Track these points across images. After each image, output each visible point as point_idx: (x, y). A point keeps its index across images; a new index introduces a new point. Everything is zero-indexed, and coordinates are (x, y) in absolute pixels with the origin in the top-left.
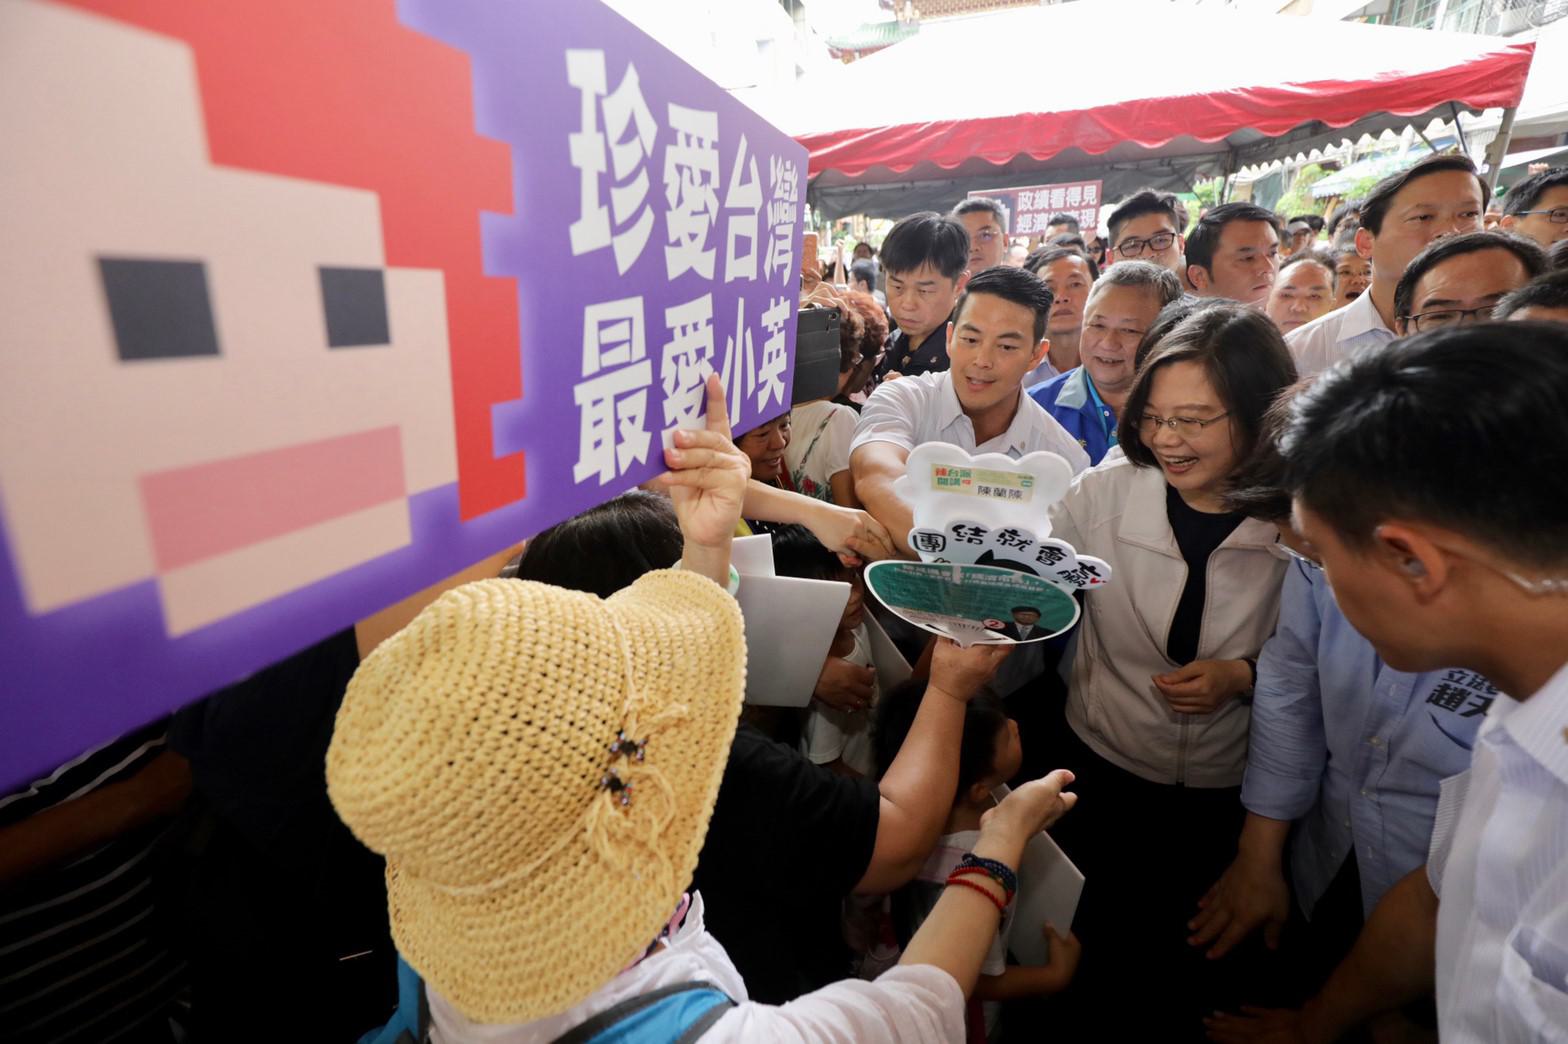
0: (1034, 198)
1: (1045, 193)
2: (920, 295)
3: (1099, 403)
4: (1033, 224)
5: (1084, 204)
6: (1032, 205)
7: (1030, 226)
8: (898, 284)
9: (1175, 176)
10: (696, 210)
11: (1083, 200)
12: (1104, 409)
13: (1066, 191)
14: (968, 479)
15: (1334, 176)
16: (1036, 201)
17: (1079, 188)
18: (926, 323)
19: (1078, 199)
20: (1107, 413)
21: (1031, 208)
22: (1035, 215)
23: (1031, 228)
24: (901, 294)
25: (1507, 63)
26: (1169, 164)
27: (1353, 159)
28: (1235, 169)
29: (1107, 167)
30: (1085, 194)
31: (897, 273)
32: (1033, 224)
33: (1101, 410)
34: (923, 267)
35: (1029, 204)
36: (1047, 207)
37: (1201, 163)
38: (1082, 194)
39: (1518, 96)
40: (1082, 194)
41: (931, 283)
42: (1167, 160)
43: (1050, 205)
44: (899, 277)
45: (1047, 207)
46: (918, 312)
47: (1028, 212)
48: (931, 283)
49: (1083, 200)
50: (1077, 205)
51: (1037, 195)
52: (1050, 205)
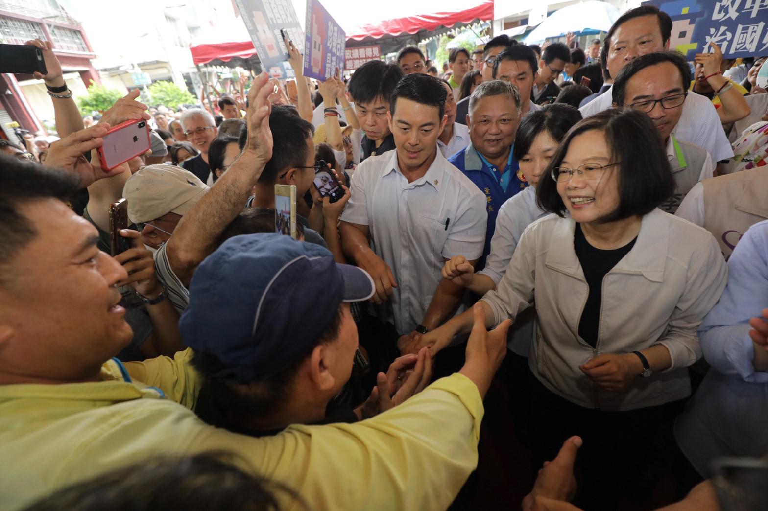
0: (352, 53)
1: (356, 51)
2: (377, 116)
3: (490, 165)
4: (353, 65)
5: (374, 56)
6: (352, 56)
7: (352, 65)
8: (362, 109)
9: (400, 45)
10: (445, 227)
11: (373, 54)
12: (492, 168)
13: (358, 51)
14: (207, 74)
15: (453, 41)
16: (353, 54)
17: (371, 49)
18: (383, 133)
19: (371, 54)
20: (495, 170)
21: (351, 58)
22: (354, 61)
23: (353, 67)
24: (365, 115)
25: (488, 6)
26: (396, 40)
27: (458, 33)
28: (420, 41)
29: (373, 43)
30: (374, 52)
31: (361, 102)
32: (353, 65)
33: (490, 169)
34: (376, 97)
35: (350, 55)
36: (358, 57)
37: (408, 39)
38: (372, 51)
39: (493, 16)
40: (372, 51)
41: (383, 107)
42: (395, 39)
43: (359, 56)
44: (362, 105)
45: (358, 57)
46: (376, 127)
47: (350, 59)
48: (383, 107)
49: (373, 54)
50: (371, 56)
51: (353, 51)
52: (359, 56)
